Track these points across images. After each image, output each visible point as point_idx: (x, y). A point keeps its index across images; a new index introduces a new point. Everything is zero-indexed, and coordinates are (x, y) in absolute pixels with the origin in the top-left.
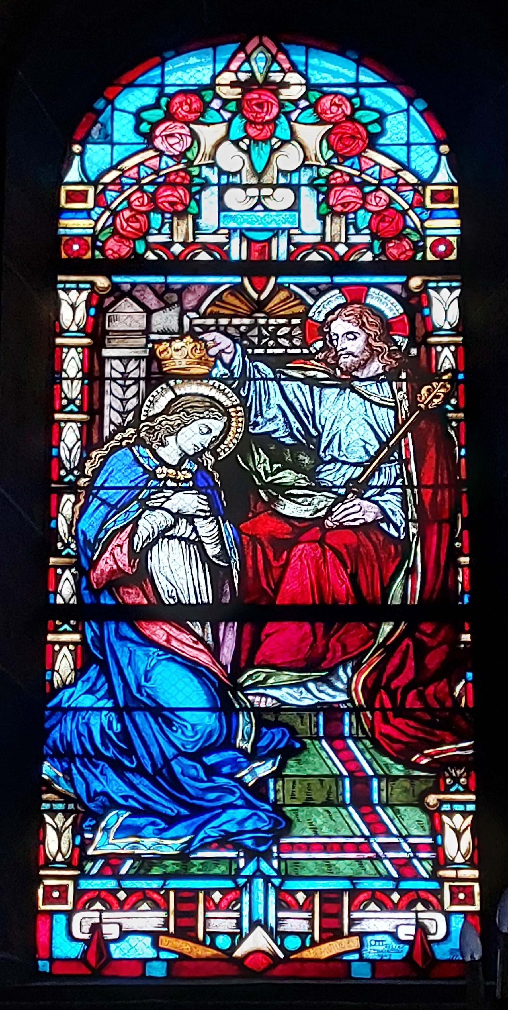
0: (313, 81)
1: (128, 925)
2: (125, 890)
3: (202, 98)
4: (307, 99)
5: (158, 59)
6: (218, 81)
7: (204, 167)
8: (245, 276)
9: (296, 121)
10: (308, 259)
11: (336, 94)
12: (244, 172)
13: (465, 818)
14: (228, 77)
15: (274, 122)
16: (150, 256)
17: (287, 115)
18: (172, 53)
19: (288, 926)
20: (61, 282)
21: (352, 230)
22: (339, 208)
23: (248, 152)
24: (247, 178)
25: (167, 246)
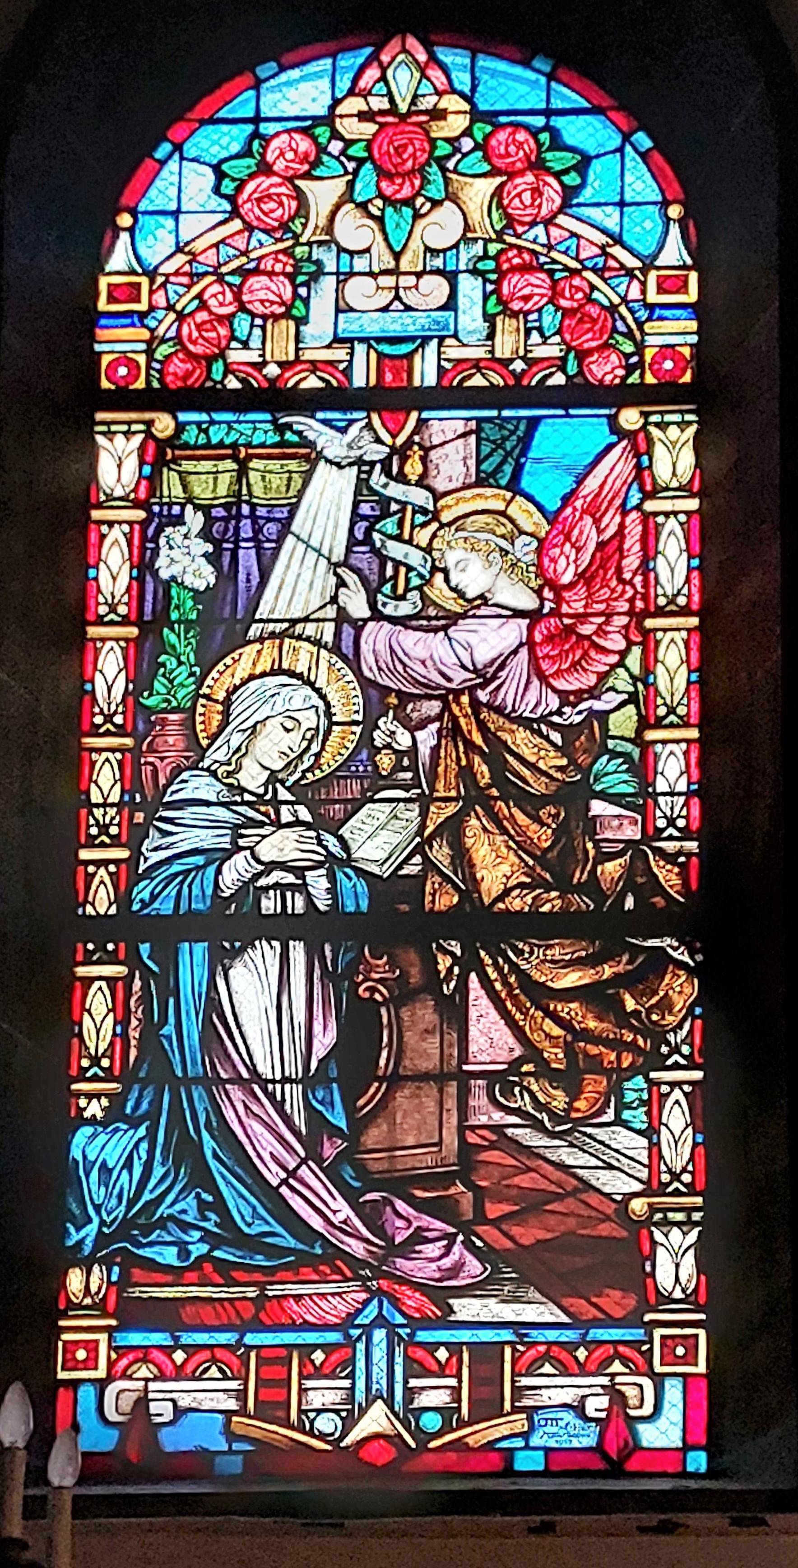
0: (483, 106)
1: (185, 1401)
2: (185, 1348)
3: (314, 139)
4: (471, 136)
5: (249, 79)
6: (338, 111)
7: (315, 246)
8: (374, 410)
9: (455, 171)
10: (468, 384)
11: (517, 126)
12: (374, 250)
13: (685, 1234)
14: (355, 104)
15: (421, 171)
16: (233, 383)
17: (441, 162)
18: (271, 67)
19: (424, 1400)
20: (102, 423)
21: (535, 337)
22: (516, 306)
23: (380, 220)
24: (382, 259)
25: (259, 366)
